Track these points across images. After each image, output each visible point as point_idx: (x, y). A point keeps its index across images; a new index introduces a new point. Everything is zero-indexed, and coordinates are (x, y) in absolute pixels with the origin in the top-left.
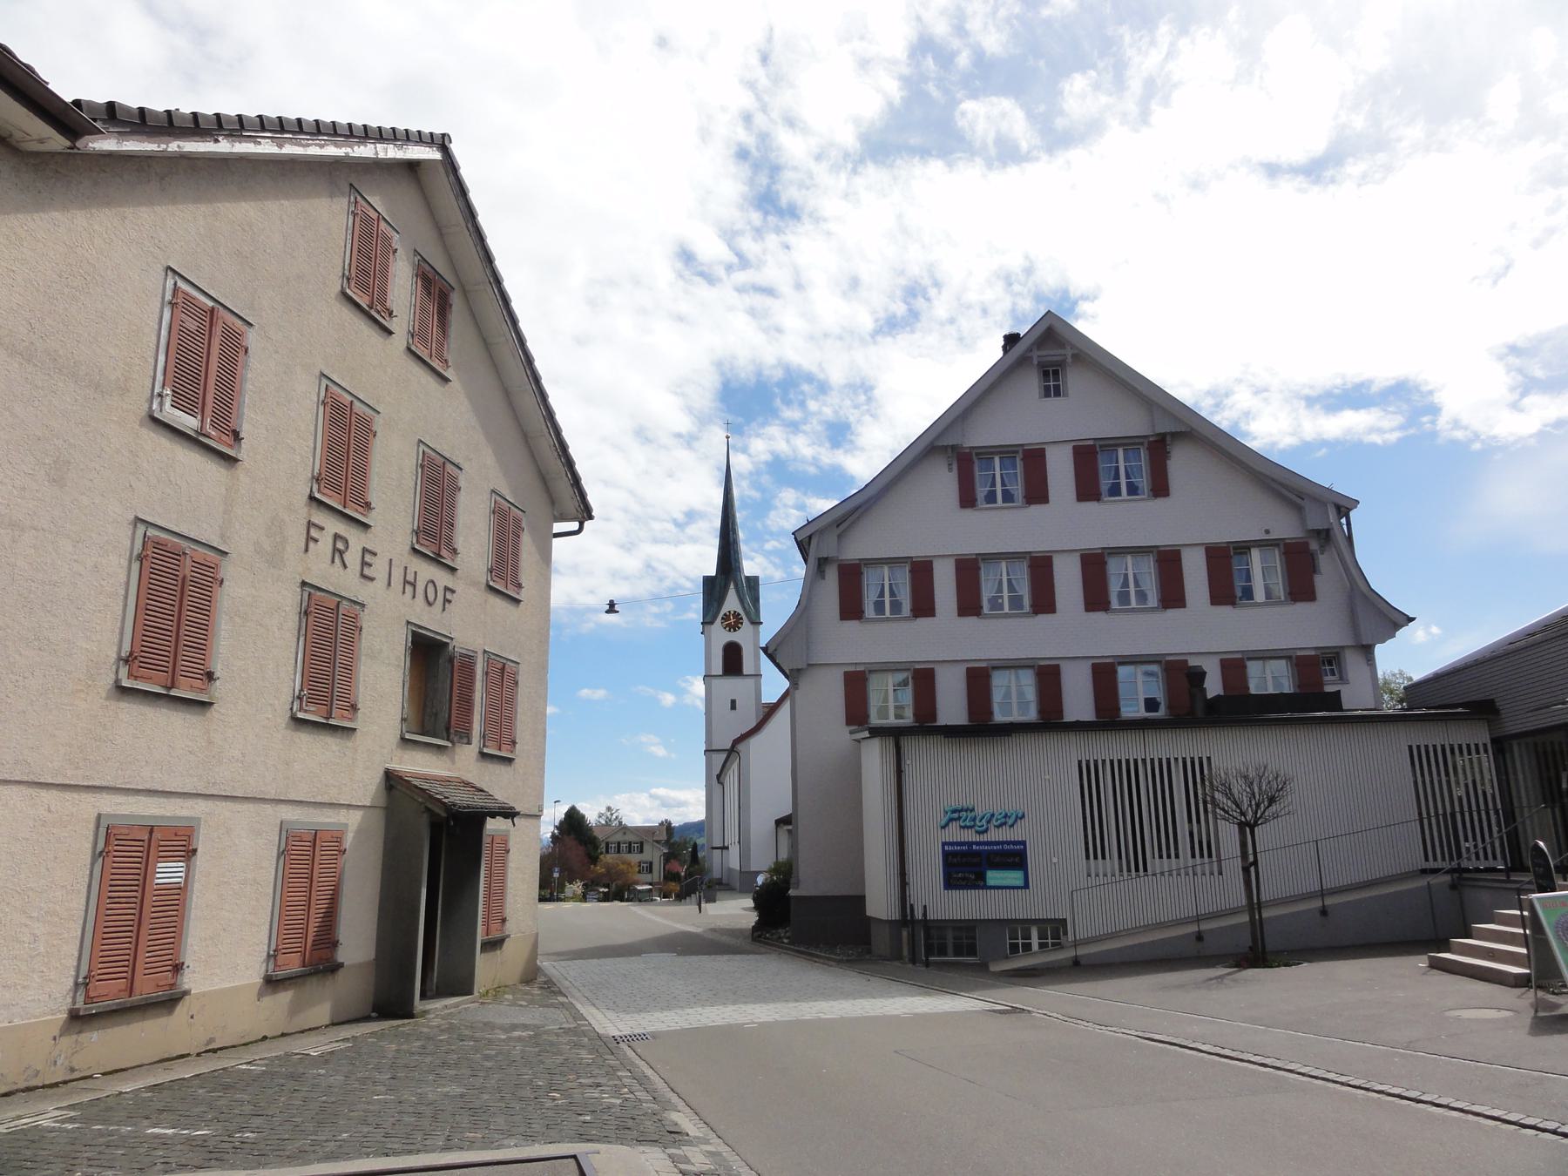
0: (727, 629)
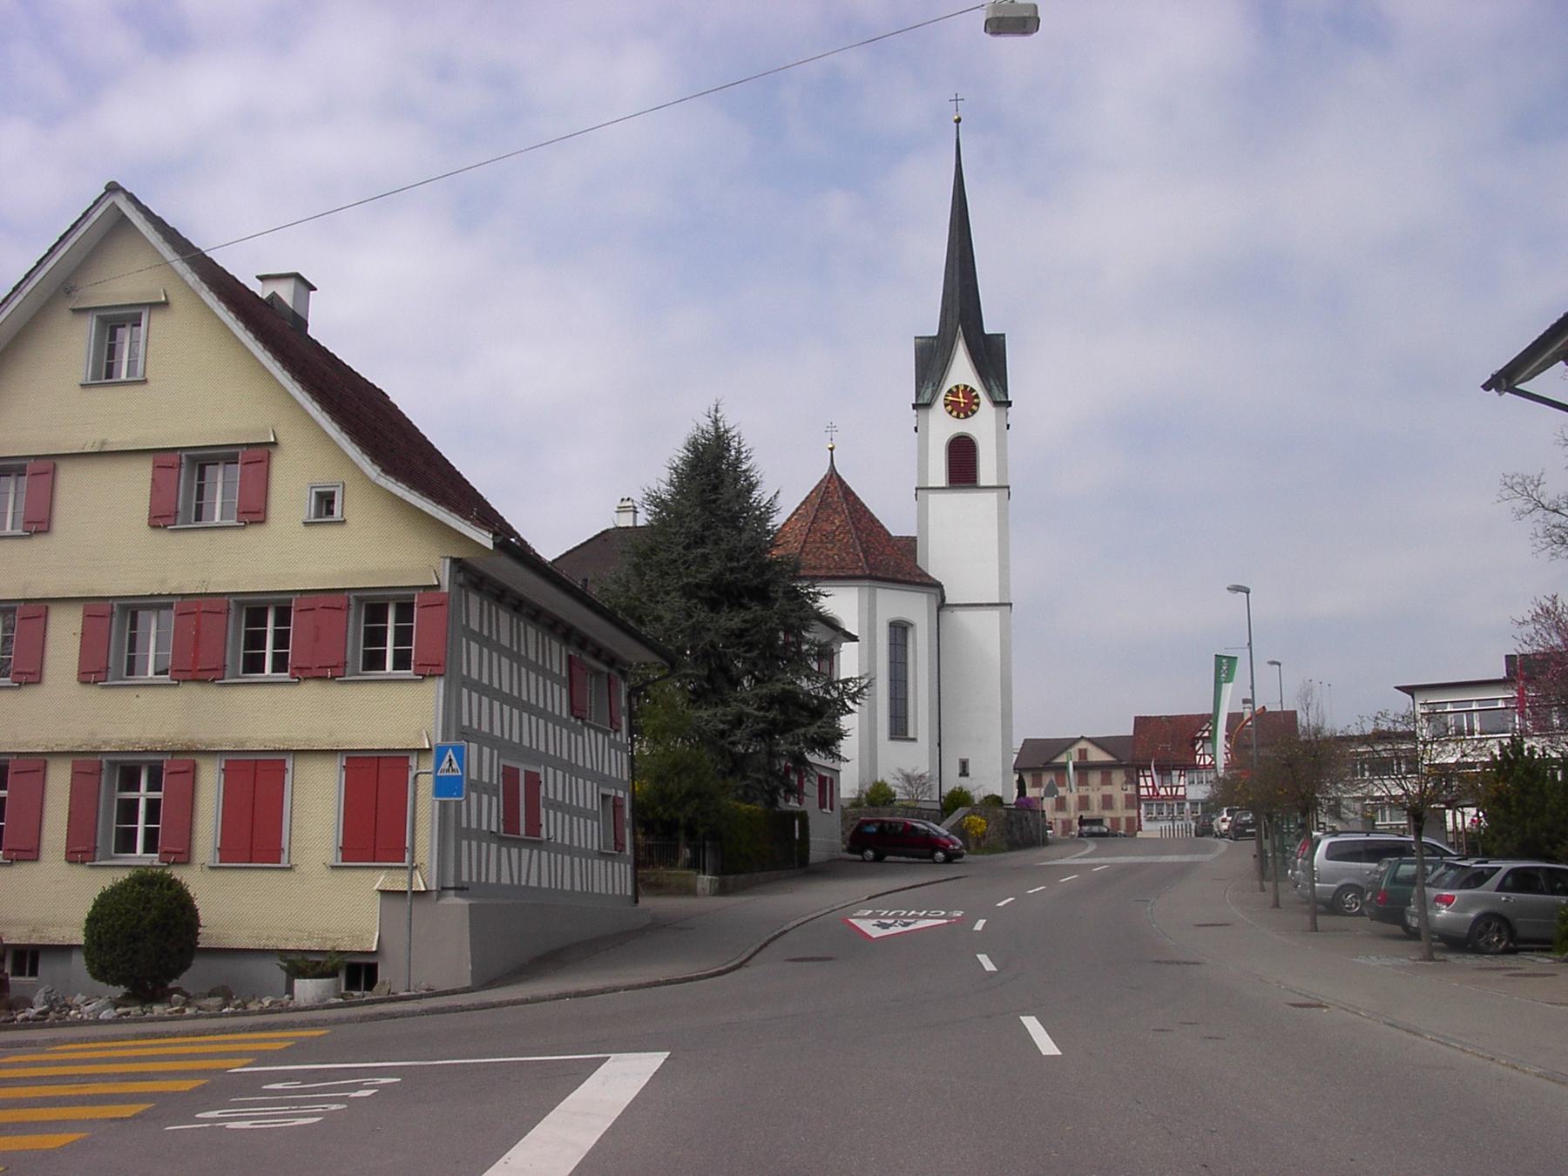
0: (949, 408)
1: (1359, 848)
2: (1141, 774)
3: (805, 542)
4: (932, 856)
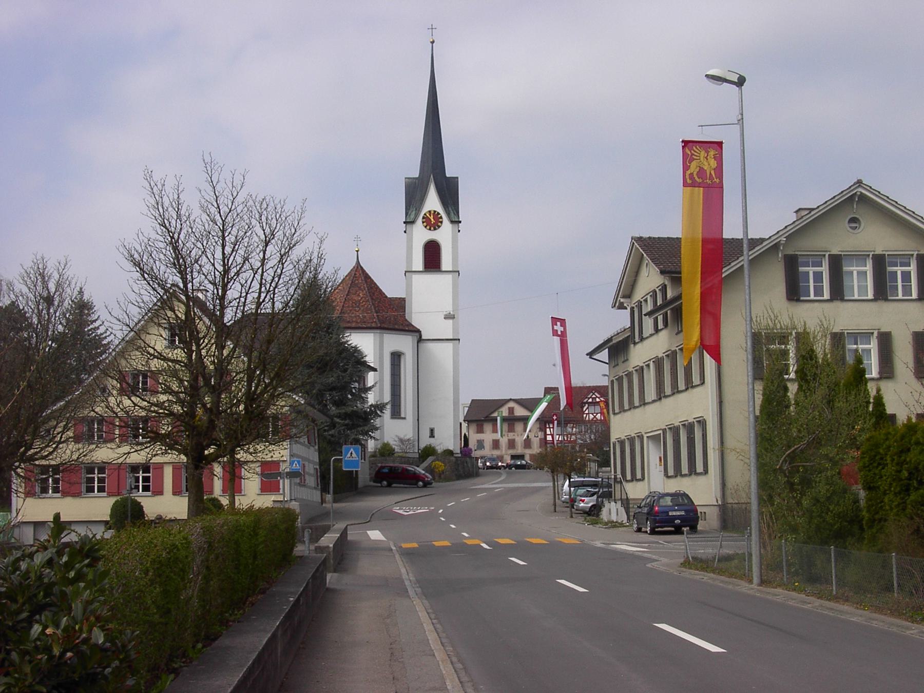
1: (592, 483)
2: (548, 426)
3: (343, 306)
4: (416, 484)
